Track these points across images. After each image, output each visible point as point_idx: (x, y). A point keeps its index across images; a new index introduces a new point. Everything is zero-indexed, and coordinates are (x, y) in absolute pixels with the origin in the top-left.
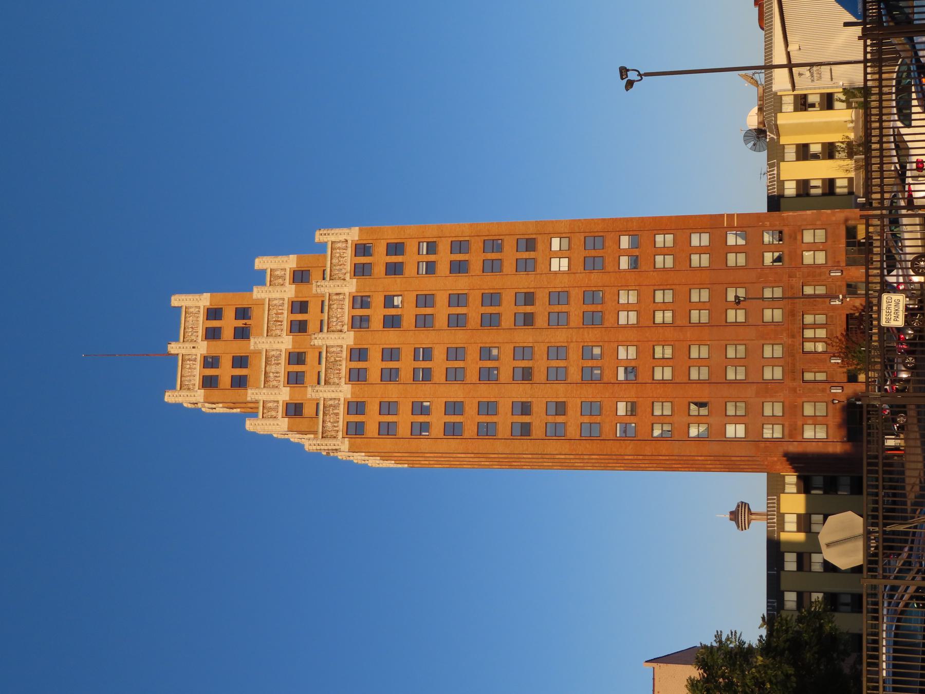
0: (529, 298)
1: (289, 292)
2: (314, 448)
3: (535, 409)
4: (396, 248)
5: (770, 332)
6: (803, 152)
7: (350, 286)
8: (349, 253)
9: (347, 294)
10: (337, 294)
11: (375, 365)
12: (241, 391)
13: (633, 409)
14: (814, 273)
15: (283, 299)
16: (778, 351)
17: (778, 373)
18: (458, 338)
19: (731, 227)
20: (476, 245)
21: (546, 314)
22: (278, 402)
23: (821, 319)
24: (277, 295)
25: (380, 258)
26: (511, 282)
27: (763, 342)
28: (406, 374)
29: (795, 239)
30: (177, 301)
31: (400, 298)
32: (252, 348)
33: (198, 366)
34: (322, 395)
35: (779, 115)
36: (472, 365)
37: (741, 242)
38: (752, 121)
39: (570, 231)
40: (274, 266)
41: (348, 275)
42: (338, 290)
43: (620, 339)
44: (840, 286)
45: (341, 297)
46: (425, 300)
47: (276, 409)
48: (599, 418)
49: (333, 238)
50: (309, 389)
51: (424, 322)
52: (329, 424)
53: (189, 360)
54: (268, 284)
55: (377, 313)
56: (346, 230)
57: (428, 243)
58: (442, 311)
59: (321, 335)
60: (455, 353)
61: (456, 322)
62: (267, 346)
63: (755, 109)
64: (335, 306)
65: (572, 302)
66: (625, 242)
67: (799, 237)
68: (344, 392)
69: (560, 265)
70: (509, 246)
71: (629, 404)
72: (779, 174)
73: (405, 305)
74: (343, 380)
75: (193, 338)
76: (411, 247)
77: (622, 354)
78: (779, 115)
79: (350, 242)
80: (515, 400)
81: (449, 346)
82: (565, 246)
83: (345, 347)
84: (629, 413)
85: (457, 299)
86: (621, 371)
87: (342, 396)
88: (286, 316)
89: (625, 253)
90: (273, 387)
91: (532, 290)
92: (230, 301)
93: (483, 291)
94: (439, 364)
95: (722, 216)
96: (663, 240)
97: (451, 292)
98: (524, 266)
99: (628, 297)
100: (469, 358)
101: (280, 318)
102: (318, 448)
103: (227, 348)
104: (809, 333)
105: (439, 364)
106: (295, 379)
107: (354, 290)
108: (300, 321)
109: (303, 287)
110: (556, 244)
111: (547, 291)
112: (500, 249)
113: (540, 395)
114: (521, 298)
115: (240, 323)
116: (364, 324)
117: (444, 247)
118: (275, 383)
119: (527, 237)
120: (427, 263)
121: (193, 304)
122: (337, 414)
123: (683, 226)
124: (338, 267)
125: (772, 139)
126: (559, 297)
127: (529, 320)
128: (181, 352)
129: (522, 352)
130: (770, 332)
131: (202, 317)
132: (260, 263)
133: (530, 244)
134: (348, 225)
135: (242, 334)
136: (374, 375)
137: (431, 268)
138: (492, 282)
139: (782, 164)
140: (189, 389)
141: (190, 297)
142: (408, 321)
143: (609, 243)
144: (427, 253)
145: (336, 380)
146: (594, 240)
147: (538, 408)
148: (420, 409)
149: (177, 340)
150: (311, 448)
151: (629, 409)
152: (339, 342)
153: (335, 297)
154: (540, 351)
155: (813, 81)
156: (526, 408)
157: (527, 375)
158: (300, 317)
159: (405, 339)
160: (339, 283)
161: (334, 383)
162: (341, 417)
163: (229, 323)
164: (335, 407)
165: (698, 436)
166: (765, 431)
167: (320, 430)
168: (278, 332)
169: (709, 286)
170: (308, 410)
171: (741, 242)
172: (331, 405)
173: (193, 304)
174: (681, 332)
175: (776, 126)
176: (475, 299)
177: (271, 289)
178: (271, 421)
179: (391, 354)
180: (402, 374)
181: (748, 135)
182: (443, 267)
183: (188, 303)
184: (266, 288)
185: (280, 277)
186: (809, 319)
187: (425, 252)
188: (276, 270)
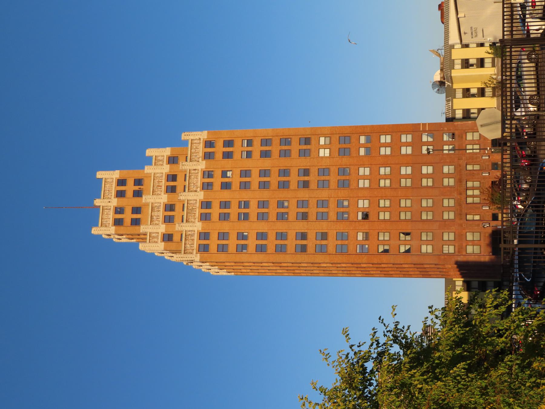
0: (306, 172)
1: (166, 169)
2: (180, 259)
3: (309, 236)
4: (229, 143)
5: (447, 192)
6: (467, 93)
7: (202, 165)
8: (201, 146)
9: (200, 170)
10: (195, 170)
11: (215, 211)
12: (137, 227)
13: (367, 236)
14: (473, 159)
15: (162, 173)
16: (452, 203)
18: (265, 195)
19: (425, 131)
20: (276, 141)
21: (317, 181)
22: (158, 233)
23: (477, 184)
24: (159, 171)
25: (219, 149)
26: (296, 163)
27: (443, 197)
29: (462, 137)
30: (100, 175)
31: (231, 172)
32: (144, 201)
33: (112, 212)
34: (184, 229)
36: (273, 211)
37: (430, 139)
38: (437, 77)
39: (331, 133)
40: (157, 154)
41: (200, 159)
42: (195, 167)
43: (360, 195)
44: (488, 165)
45: (197, 171)
46: (246, 173)
47: (157, 237)
48: (347, 241)
49: (192, 137)
50: (177, 225)
51: (245, 186)
52: (188, 246)
53: (106, 209)
54: (154, 164)
55: (217, 181)
56: (199, 133)
57: (248, 140)
58: (255, 179)
59: (184, 193)
60: (263, 204)
61: (264, 186)
63: (439, 71)
64: (193, 177)
65: (331, 174)
66: (363, 139)
67: (464, 137)
68: (197, 226)
71: (364, 234)
72: (452, 106)
73: (234, 176)
74: (197, 220)
75: (109, 196)
76: (238, 143)
79: (202, 140)
80: (298, 231)
83: (198, 200)
84: (364, 239)
85: (264, 173)
87: (196, 229)
88: (164, 183)
89: (363, 146)
90: (156, 224)
91: (308, 168)
92: (131, 175)
94: (253, 211)
95: (419, 124)
96: (385, 139)
97: (261, 169)
98: (304, 153)
99: (365, 171)
100: (271, 207)
102: (182, 259)
103: (129, 202)
104: (470, 193)
105: (253, 211)
106: (169, 220)
108: (172, 186)
110: (322, 141)
111: (317, 168)
112: (289, 143)
113: (312, 228)
114: (302, 172)
115: (137, 188)
116: (210, 187)
117: (257, 143)
118: (157, 222)
119: (305, 136)
120: (247, 152)
121: (109, 177)
122: (193, 240)
123: (396, 130)
124: (195, 154)
125: (448, 85)
126: (324, 171)
127: (306, 185)
128: (102, 204)
129: (302, 203)
130: (447, 192)
131: (114, 184)
132: (150, 152)
133: (307, 141)
134: (201, 130)
135: (138, 194)
137: (249, 155)
138: (284, 163)
139: (454, 100)
140: (106, 226)
141: (108, 172)
142: (235, 185)
143: (353, 140)
144: (247, 146)
145: (193, 220)
146: (344, 139)
147: (311, 236)
148: (241, 236)
149: (99, 197)
151: (364, 236)
152: (195, 198)
153: (193, 172)
154: (313, 203)
155: (472, 37)
156: (304, 236)
157: (305, 216)
158: (172, 184)
159: (234, 196)
160: (195, 163)
161: (192, 222)
162: (195, 241)
163: (130, 188)
164: (192, 235)
166: (444, 249)
167: (183, 249)
168: (159, 192)
170: (176, 238)
171: (430, 139)
172: (190, 235)
173: (109, 177)
175: (451, 77)
176: (275, 172)
177: (155, 167)
178: (154, 244)
179: (225, 205)
181: (434, 84)
182: (256, 154)
183: (107, 176)
185: (161, 161)
186: (470, 184)
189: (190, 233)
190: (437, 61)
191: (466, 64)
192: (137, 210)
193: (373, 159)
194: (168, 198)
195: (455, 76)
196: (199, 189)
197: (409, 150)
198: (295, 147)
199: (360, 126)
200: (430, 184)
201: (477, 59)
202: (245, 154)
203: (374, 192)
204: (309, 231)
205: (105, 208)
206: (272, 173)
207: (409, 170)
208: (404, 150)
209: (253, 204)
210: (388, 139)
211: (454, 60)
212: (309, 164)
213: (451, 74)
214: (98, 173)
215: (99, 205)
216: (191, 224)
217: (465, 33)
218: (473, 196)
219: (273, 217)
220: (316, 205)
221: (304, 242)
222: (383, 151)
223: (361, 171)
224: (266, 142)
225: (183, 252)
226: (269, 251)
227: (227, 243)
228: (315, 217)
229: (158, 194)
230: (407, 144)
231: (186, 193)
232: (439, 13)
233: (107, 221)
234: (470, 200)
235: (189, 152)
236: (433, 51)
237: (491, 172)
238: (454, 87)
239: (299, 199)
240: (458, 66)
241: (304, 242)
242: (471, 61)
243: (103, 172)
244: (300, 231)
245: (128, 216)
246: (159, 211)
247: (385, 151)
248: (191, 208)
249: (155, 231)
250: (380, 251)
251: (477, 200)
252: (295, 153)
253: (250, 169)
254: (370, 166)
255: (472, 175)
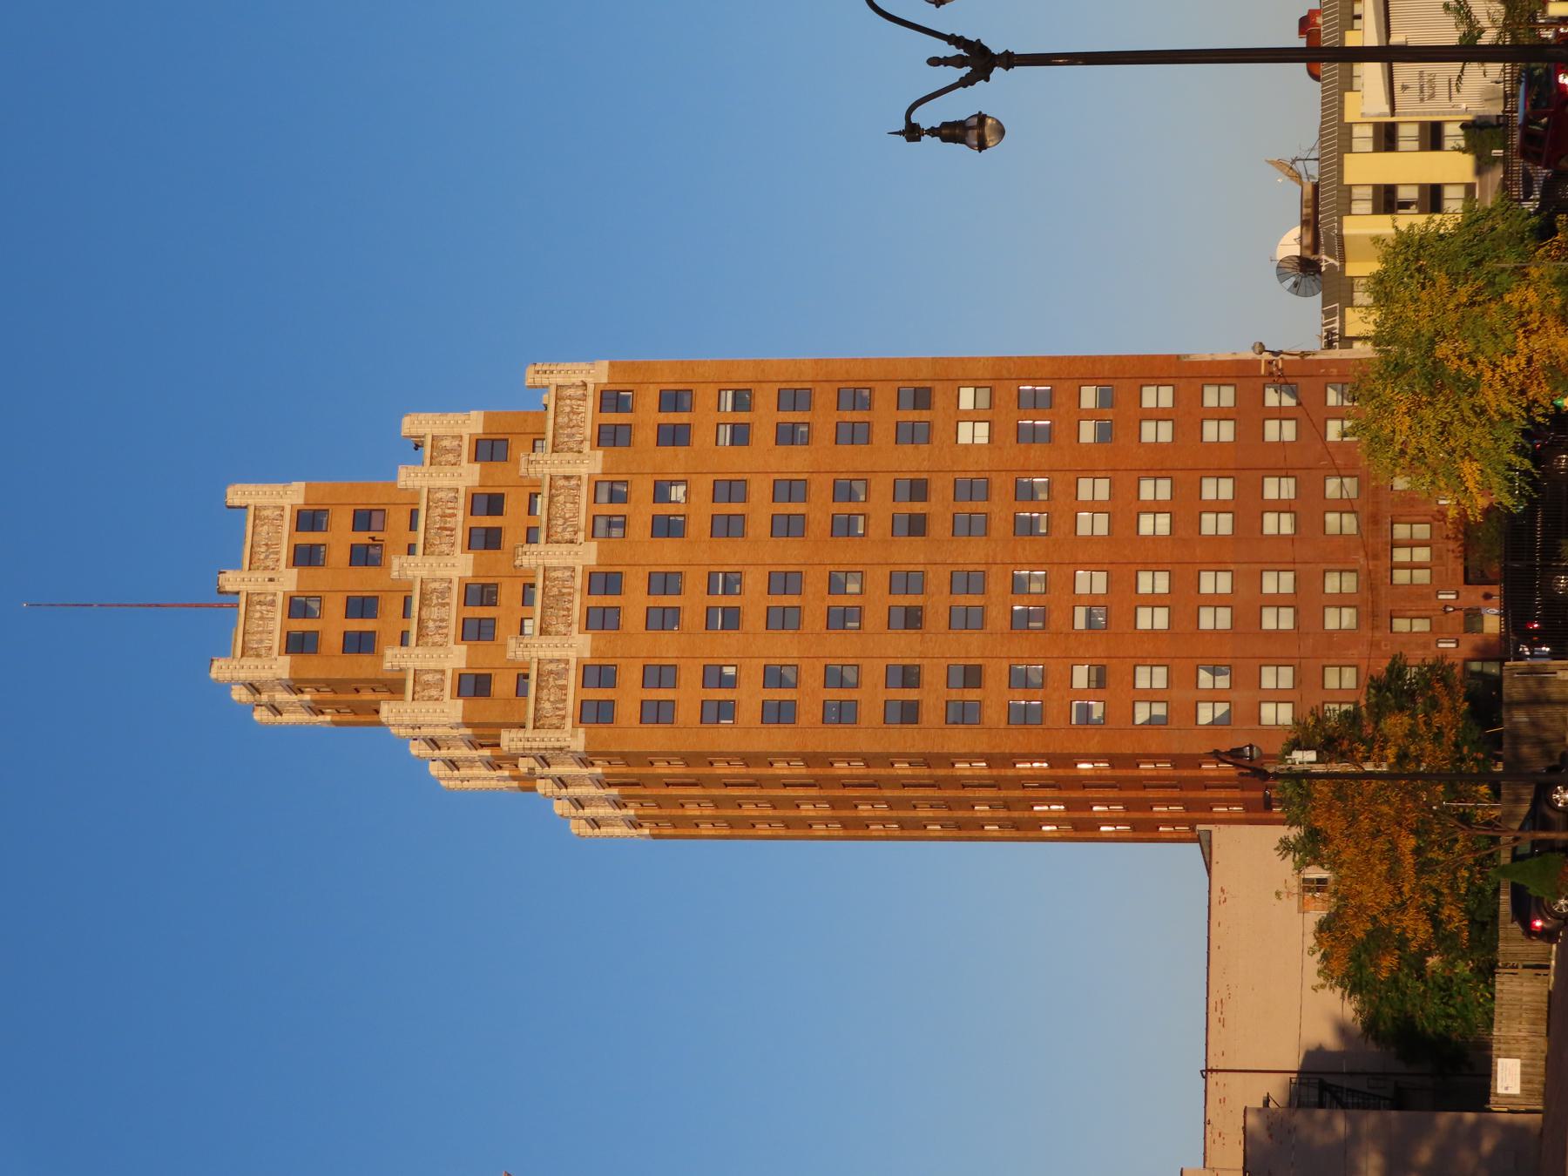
0: (919, 490)
1: (469, 475)
2: (520, 745)
3: (926, 677)
7: (592, 463)
9: (585, 478)
10: (567, 478)
11: (635, 601)
12: (365, 659)
13: (1100, 680)
16: (1350, 583)
17: (1348, 618)
18: (790, 553)
20: (825, 397)
22: (443, 672)
23: (1422, 531)
24: (446, 483)
27: (1324, 566)
28: (693, 616)
30: (237, 495)
32: (395, 574)
35: (1346, 219)
36: (814, 601)
38: (1290, 244)
39: (998, 377)
41: (587, 445)
42: (568, 471)
43: (1081, 558)
45: (573, 482)
46: (730, 489)
47: (440, 685)
51: (728, 527)
52: (547, 705)
54: (427, 461)
55: (641, 510)
56: (584, 366)
57: (736, 392)
58: (760, 508)
60: (783, 582)
61: (786, 527)
62: (424, 574)
63: (1296, 231)
64: (561, 498)
65: (995, 498)
66: (1089, 397)
68: (578, 646)
69: (973, 434)
70: (884, 398)
71: (1093, 670)
72: (1342, 328)
73: (693, 498)
74: (575, 627)
75: (270, 563)
76: (704, 398)
77: (1082, 587)
78: (1346, 219)
79: (591, 387)
80: (892, 662)
81: (773, 569)
82: (984, 402)
83: (579, 569)
84: (1093, 685)
85: (788, 489)
86: (1080, 613)
88: (460, 520)
89: (1089, 415)
90: (434, 644)
91: (924, 476)
93: (835, 476)
96: (1157, 397)
97: (777, 476)
98: (909, 434)
99: (1095, 489)
100: (808, 589)
101: (450, 523)
102: (528, 745)
104: (1401, 555)
107: (598, 470)
108: (487, 529)
109: (497, 466)
110: (967, 398)
111: (951, 477)
112: (868, 405)
113: (937, 651)
114: (904, 490)
115: (363, 538)
117: (765, 399)
118: (437, 638)
119: (917, 384)
120: (734, 426)
122: (564, 688)
125: (1331, 266)
126: (972, 488)
127: (917, 526)
129: (905, 581)
130: (1337, 554)
132: (413, 424)
133: (922, 398)
136: (634, 617)
137: (741, 435)
138: (852, 459)
139: (1348, 311)
140: (258, 656)
142: (699, 525)
144: (734, 409)
146: (1036, 391)
147: (933, 676)
148: (714, 676)
150: (513, 745)
151: (1093, 677)
152: (570, 562)
153: (562, 483)
154: (938, 579)
155: (1422, 100)
156: (909, 676)
157: (913, 619)
159: (692, 556)
161: (557, 633)
163: (339, 537)
165: (1213, 723)
168: (445, 548)
169: (1233, 473)
170: (503, 685)
171: (1289, 401)
172: (551, 672)
174: (1184, 555)
175: (1341, 237)
178: (431, 705)
179: (664, 582)
180: (686, 617)
182: (764, 433)
183: (261, 500)
184: (424, 470)
186: (1401, 531)
187: (729, 408)
188: (443, 438)
189: (552, 667)
190: (1291, 199)
191: (1387, 200)
192: (361, 606)
193: (1122, 460)
194: (476, 564)
195: (1355, 237)
196: (581, 536)
197: (1227, 431)
198: (885, 416)
199: (1082, 358)
200: (1287, 528)
201: (1422, 187)
202: (726, 434)
203: (1123, 554)
204: (925, 662)
205: (256, 598)
206: (813, 488)
207: (1226, 489)
208: (1146, 525)
209: (755, 581)
210: (1166, 397)
211: (1350, 186)
212: (926, 465)
213: (1340, 228)
214: (230, 490)
215: (235, 589)
216: (557, 640)
217: (1404, 88)
218: (1412, 566)
219: (814, 618)
220: (947, 589)
221: (911, 695)
222: (1148, 431)
223: (1085, 486)
224: (794, 398)
225: (530, 725)
226: (803, 720)
227: (672, 697)
228: (944, 623)
229: (441, 554)
230: (1220, 415)
231: (541, 547)
232: (1018, 70)
233: (261, 641)
234: (1401, 576)
235: (550, 423)
236: (1279, 164)
237: (1463, 594)
238: (1348, 274)
239: (897, 568)
240: (1362, 206)
241: (911, 695)
242: (1404, 194)
243: (251, 487)
244: (900, 662)
245: (333, 625)
246: (443, 605)
247: (1157, 433)
248: (555, 591)
249: (432, 665)
250: (1138, 721)
251: (1422, 576)
252: (883, 431)
253: (745, 477)
254: (1111, 473)
255: (1408, 508)
